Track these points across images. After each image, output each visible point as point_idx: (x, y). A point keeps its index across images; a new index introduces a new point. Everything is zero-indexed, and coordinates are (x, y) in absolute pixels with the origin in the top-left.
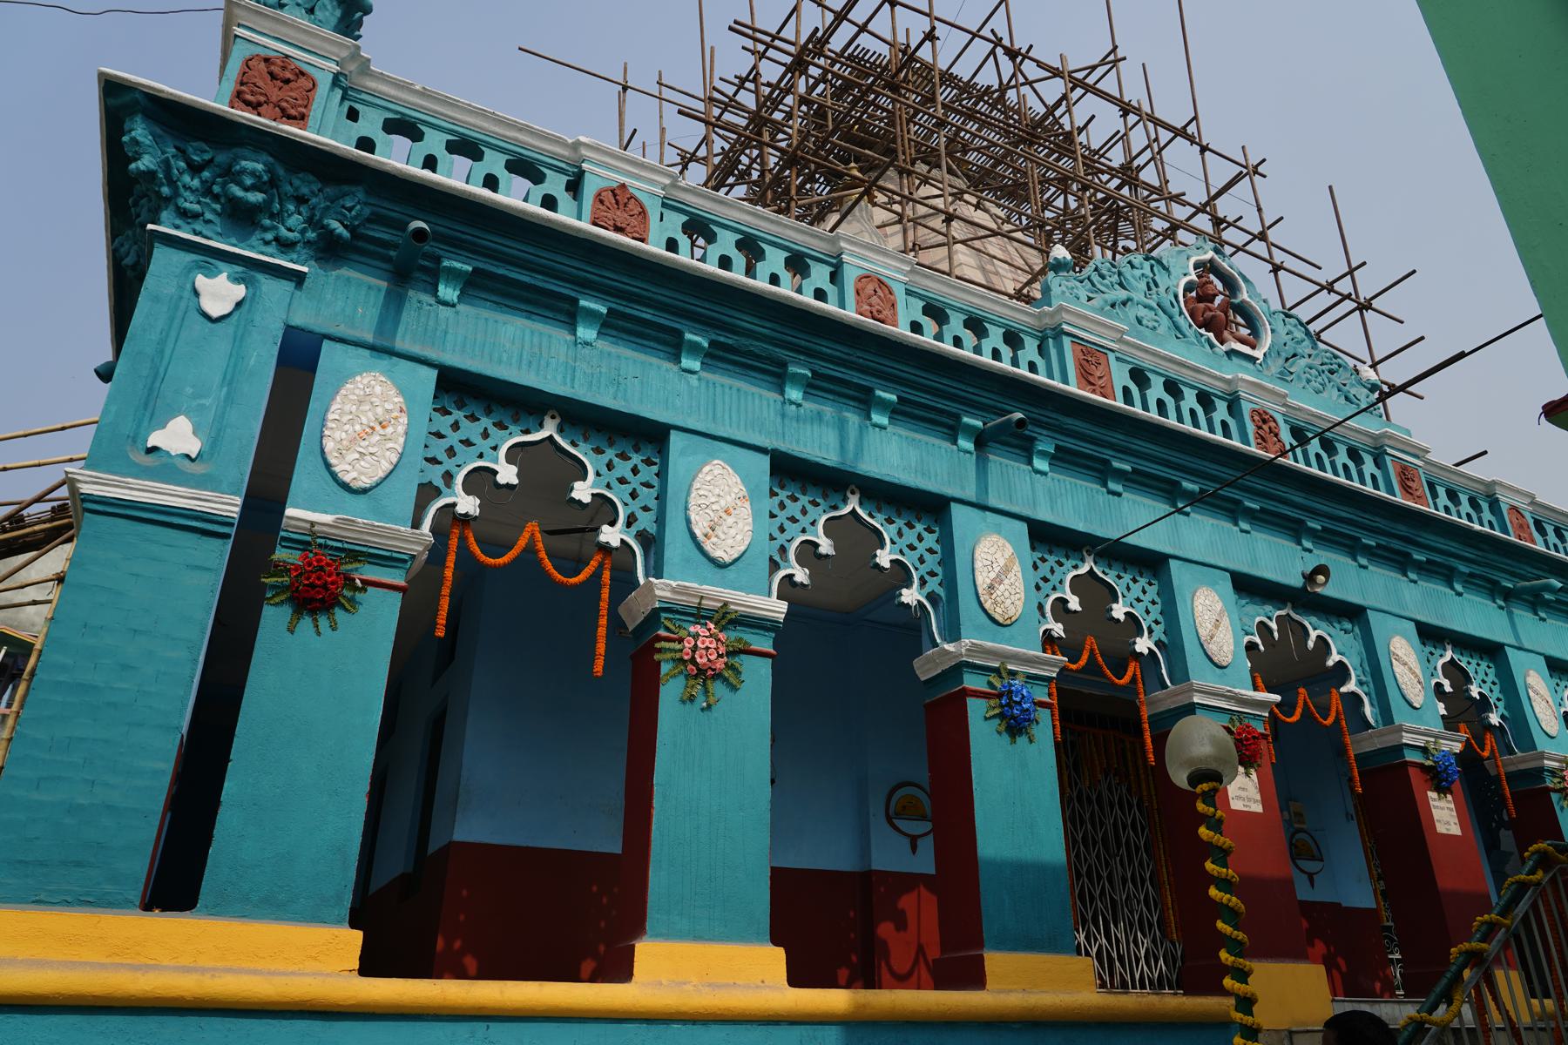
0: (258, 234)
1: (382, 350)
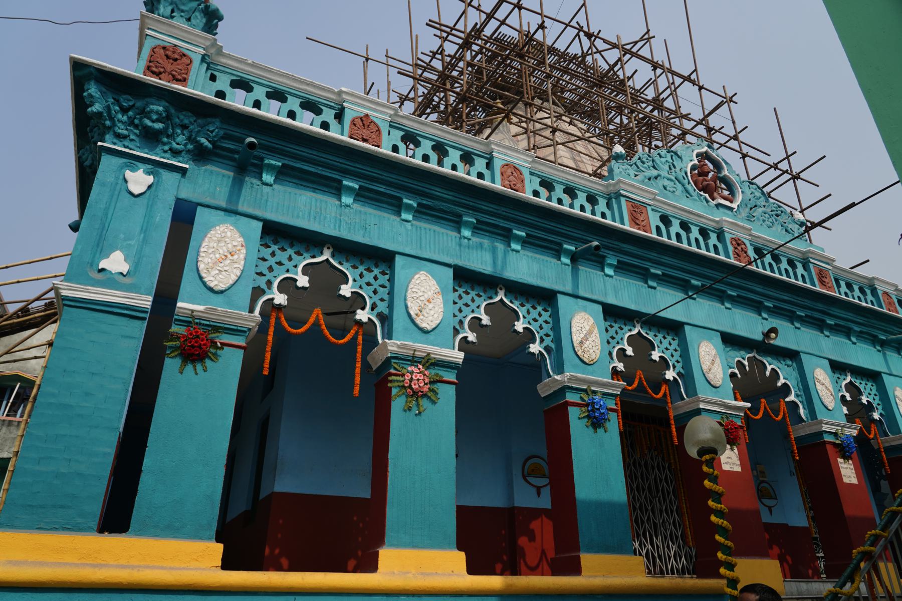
0: (160, 147)
1: (231, 211)
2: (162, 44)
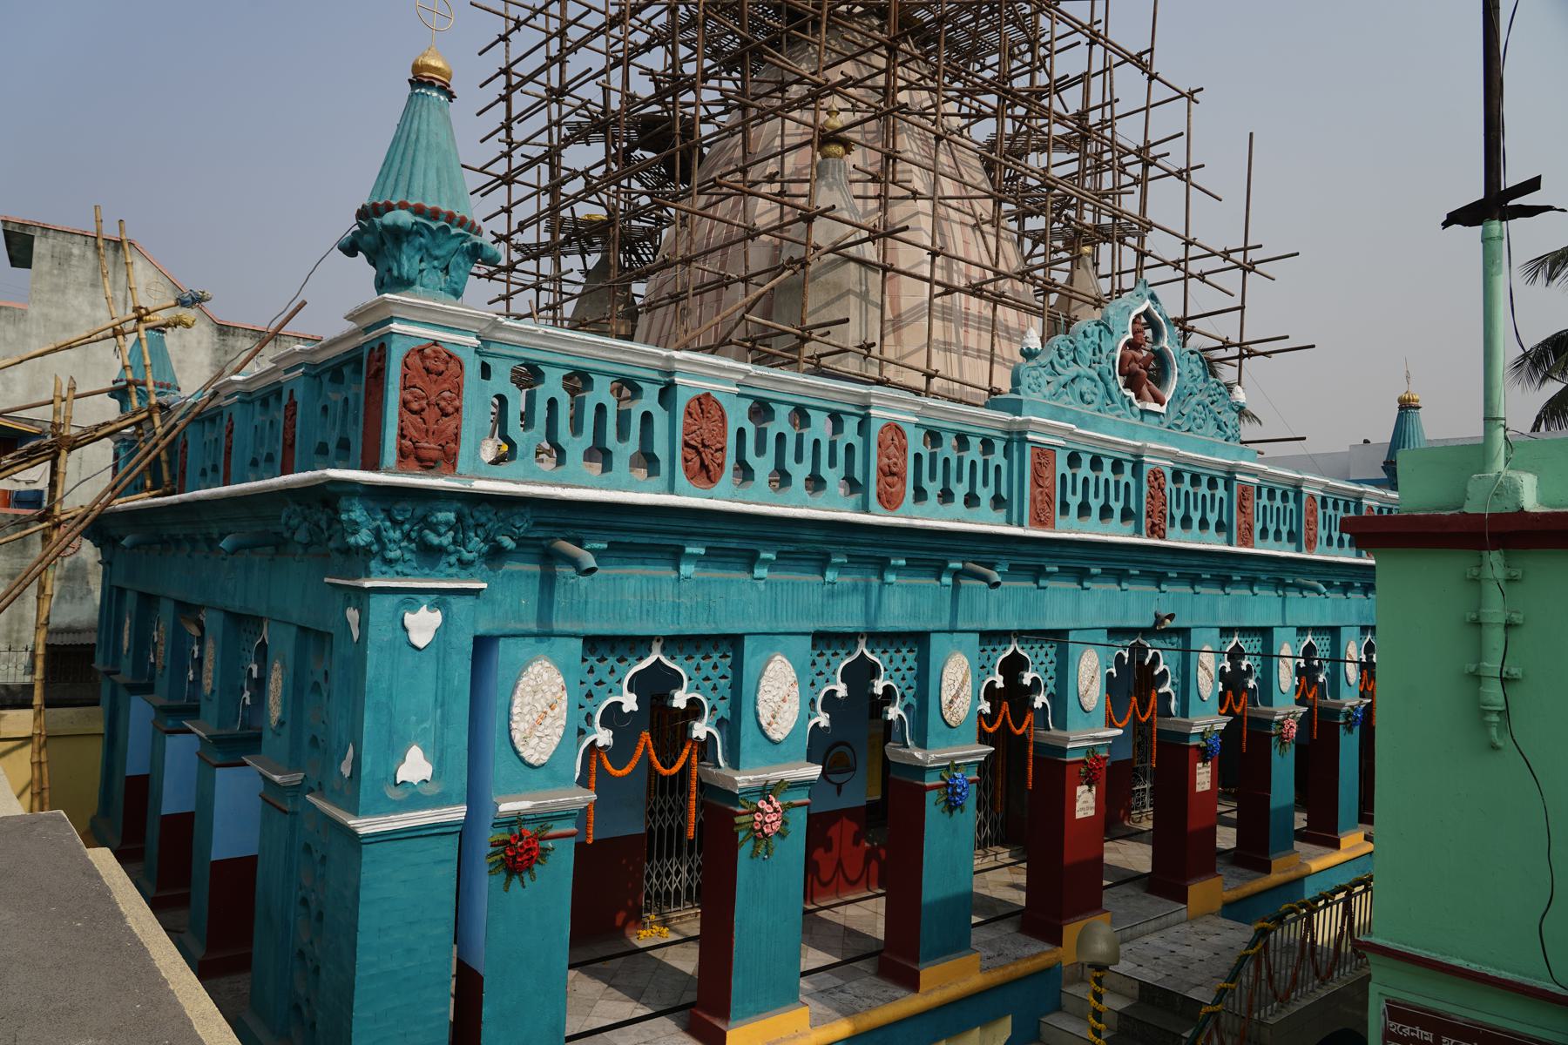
0: (444, 559)
2: (414, 344)
